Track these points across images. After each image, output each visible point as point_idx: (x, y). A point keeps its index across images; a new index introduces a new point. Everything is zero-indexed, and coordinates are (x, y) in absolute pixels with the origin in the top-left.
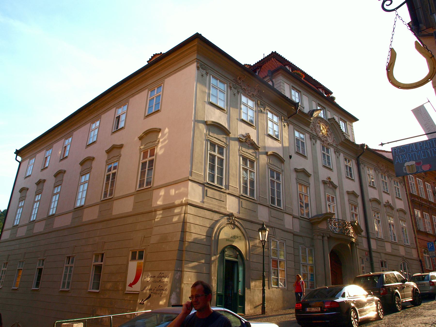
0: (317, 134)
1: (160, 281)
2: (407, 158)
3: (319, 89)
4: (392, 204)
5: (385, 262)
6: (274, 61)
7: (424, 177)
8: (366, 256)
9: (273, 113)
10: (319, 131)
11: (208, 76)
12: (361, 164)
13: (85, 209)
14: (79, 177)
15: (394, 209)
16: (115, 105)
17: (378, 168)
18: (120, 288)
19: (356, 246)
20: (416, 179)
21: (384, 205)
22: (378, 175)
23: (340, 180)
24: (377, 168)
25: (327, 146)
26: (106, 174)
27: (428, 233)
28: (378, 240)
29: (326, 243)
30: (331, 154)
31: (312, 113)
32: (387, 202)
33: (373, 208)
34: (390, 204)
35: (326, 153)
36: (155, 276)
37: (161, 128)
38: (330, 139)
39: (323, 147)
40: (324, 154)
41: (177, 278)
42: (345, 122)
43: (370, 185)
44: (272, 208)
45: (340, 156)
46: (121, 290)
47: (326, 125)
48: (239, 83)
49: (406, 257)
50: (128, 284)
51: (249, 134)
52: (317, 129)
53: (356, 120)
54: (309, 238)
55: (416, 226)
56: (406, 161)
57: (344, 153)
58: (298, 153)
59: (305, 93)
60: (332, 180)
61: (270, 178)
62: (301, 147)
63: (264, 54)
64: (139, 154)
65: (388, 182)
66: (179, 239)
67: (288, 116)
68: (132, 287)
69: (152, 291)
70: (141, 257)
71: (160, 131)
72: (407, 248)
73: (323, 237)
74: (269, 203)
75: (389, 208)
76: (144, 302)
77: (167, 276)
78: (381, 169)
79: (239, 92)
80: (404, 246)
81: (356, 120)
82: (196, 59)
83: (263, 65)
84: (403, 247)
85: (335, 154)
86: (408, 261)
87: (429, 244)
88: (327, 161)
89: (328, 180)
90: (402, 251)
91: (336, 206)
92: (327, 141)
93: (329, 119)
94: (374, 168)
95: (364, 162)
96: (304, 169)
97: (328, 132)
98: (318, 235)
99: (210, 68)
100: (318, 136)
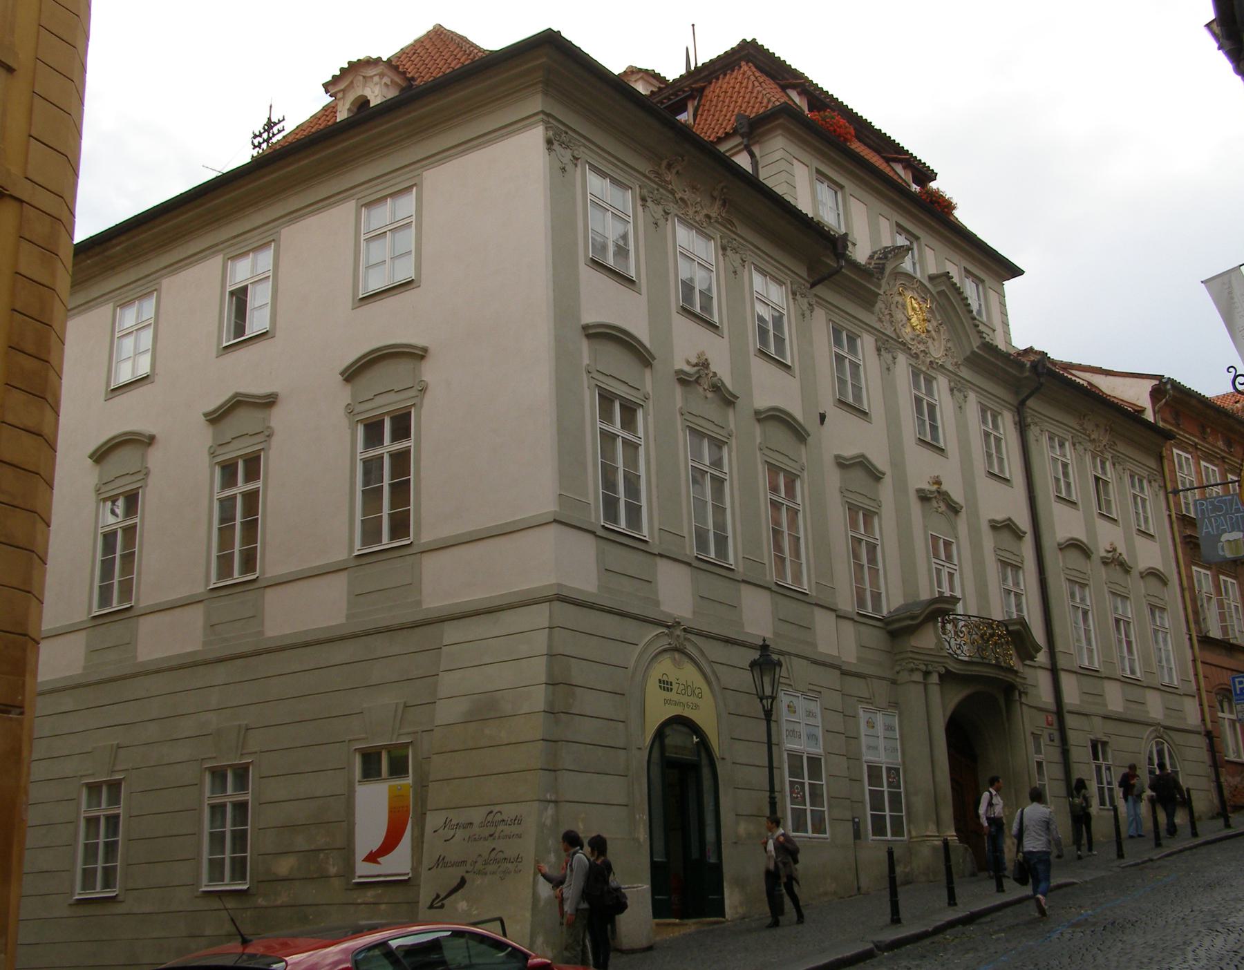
0: (896, 333)
1: (491, 835)
2: (1227, 525)
3: (893, 165)
4: (1125, 556)
5: (1104, 744)
6: (752, 78)
7: (1223, 458)
8: (1049, 727)
9: (767, 272)
10: (904, 322)
11: (579, 170)
12: (1032, 427)
13: (141, 619)
14: (93, 506)
15: (1094, 557)
16: (217, 245)
17: (1083, 436)
18: (333, 870)
19: (1020, 697)
20: (1199, 464)
21: (1102, 558)
22: (1081, 459)
23: (969, 484)
24: (1080, 434)
25: (928, 372)
26: (216, 498)
27: (1232, 645)
28: (1087, 673)
29: (935, 691)
30: (939, 396)
31: (881, 262)
32: (1111, 550)
33: (1068, 572)
34: (1120, 554)
35: (926, 395)
36: (471, 824)
37: (427, 345)
38: (937, 346)
39: (837, 333)
40: (840, 359)
41: (548, 822)
42: (978, 281)
43: (1059, 495)
44: (782, 594)
45: (895, 363)
46: (335, 876)
47: (923, 298)
48: (665, 181)
49: (1169, 723)
50: (361, 851)
51: (703, 353)
52: (898, 316)
53: (1015, 272)
54: (884, 679)
55: (1197, 622)
56: (1224, 531)
57: (980, 390)
58: (842, 403)
59: (858, 192)
60: (944, 487)
61: (599, 426)
62: (849, 382)
63: (693, 25)
64: (349, 431)
65: (1112, 480)
66: (541, 706)
67: (811, 280)
68: (378, 863)
69: (469, 868)
70: (398, 768)
71: (423, 354)
72: (1171, 697)
73: (927, 674)
74: (597, 517)
75: (1117, 567)
76: (444, 902)
77: (515, 820)
78: (1093, 437)
79: (668, 214)
80: (1159, 689)
81: (1015, 272)
82: (542, 112)
83: (710, 83)
84: (766, 593)
85: (953, 399)
86: (1170, 737)
87: (1237, 680)
88: (852, 383)
89: (935, 488)
90: (1155, 707)
91: (958, 571)
92: (927, 354)
93: (932, 278)
94: (1072, 437)
95: (1042, 419)
96: (863, 456)
97: (929, 321)
98: (912, 670)
99: (583, 141)
100: (899, 338)
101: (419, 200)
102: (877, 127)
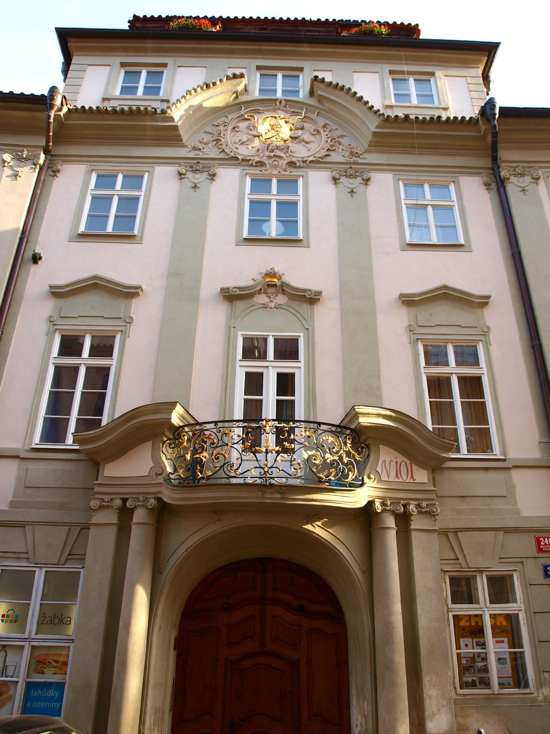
96: (445, 287)
97: (302, 128)
102: (315, 19)
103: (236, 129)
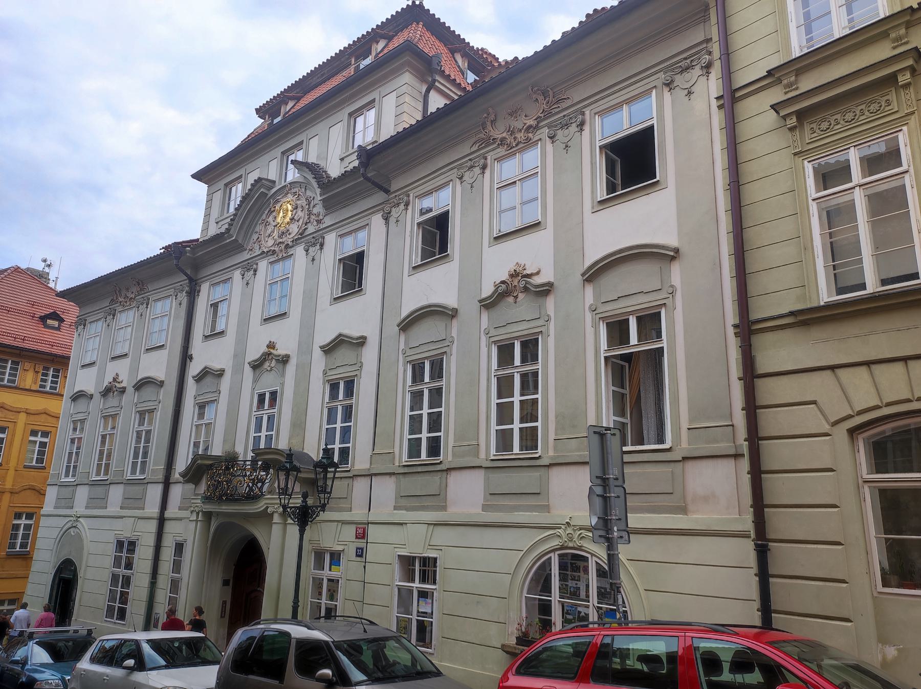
101: (369, 235)
103: (267, 224)
